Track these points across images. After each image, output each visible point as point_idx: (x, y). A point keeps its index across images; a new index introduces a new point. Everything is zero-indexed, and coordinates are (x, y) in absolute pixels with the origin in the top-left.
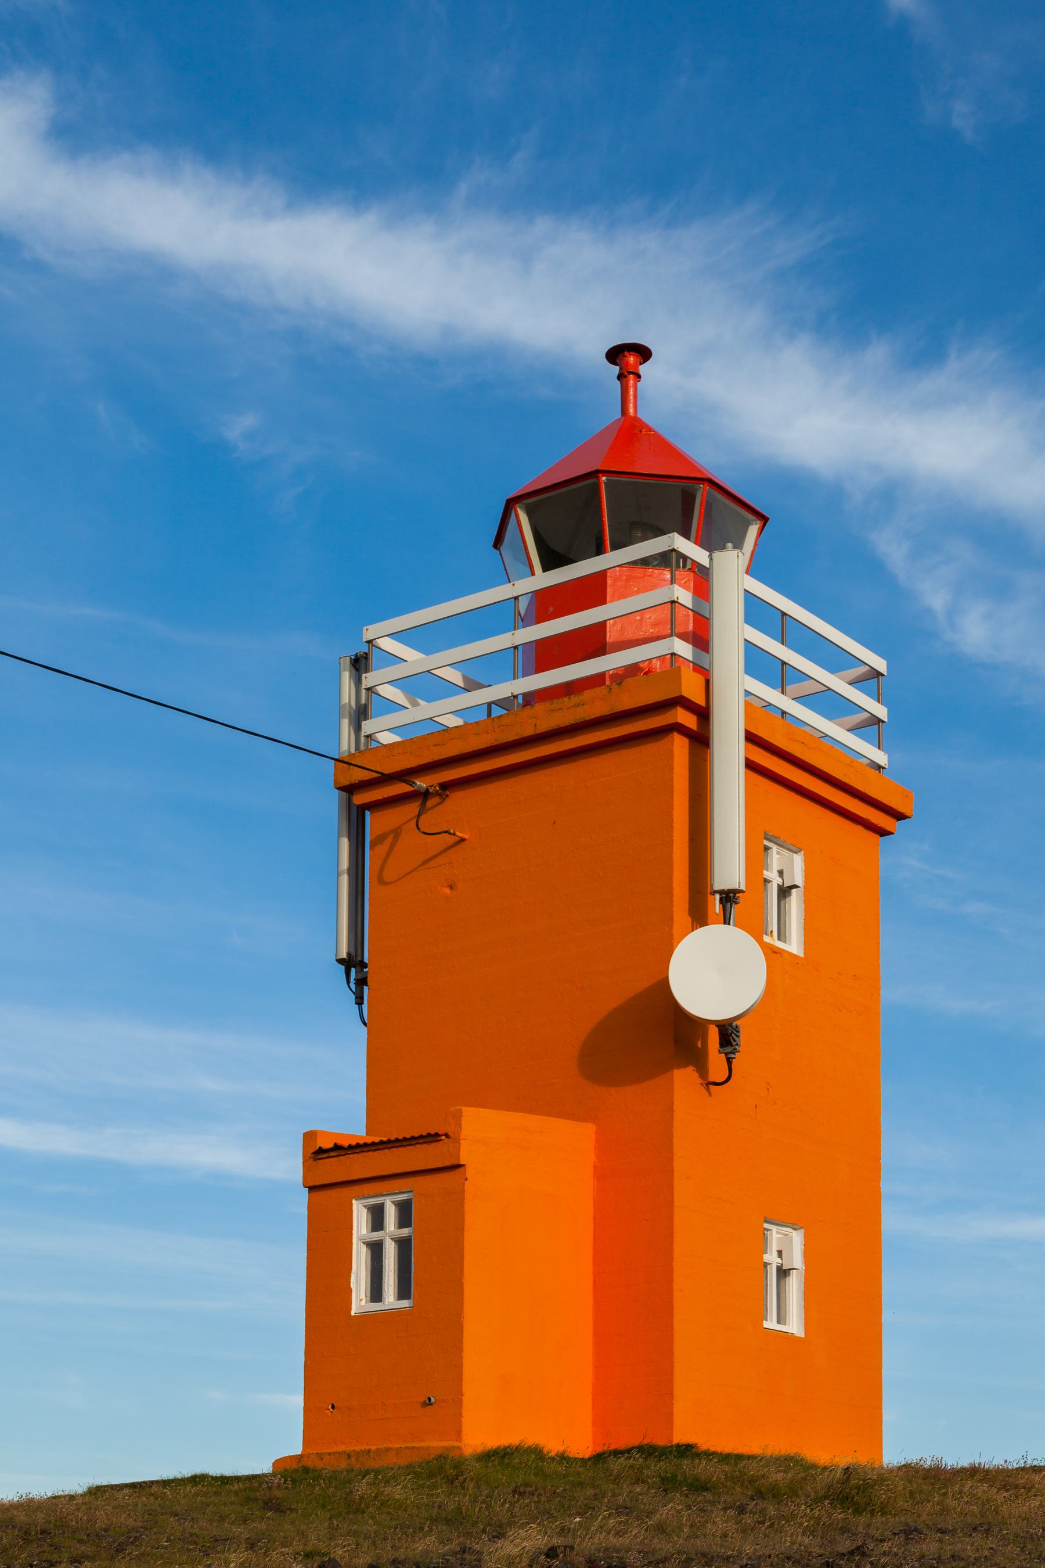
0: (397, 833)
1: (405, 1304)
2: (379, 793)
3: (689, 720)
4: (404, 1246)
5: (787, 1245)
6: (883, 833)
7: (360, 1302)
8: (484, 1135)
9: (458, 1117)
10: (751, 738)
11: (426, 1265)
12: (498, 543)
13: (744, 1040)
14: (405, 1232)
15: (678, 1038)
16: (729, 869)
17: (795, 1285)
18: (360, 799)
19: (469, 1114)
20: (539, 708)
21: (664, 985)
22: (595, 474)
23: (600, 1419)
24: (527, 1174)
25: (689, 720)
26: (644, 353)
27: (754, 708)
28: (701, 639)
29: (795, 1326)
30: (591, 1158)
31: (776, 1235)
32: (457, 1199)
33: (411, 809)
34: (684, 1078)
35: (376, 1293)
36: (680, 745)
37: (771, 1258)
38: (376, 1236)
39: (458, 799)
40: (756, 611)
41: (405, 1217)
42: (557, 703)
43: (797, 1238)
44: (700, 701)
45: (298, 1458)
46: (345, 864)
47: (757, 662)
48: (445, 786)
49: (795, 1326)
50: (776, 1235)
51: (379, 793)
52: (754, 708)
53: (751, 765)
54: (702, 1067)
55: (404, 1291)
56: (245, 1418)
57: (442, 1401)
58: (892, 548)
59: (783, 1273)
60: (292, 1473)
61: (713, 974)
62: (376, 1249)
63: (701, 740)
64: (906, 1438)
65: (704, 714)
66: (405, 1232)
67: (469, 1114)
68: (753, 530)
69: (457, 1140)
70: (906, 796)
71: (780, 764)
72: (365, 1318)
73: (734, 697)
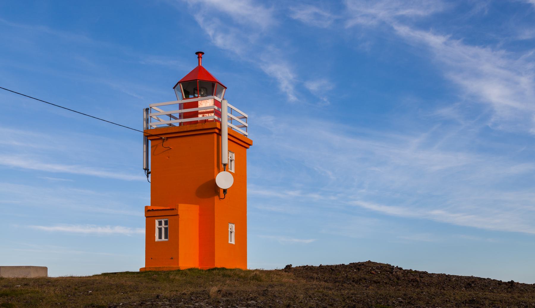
0: (157, 145)
1: (166, 240)
2: (151, 136)
3: (217, 131)
4: (166, 229)
5: (232, 227)
6: (247, 148)
7: (157, 239)
8: (182, 209)
9: (178, 206)
10: (229, 134)
11: (171, 232)
12: (174, 88)
13: (228, 191)
14: (166, 226)
15: (214, 189)
16: (225, 160)
17: (233, 234)
18: (149, 138)
19: (180, 205)
20: (188, 126)
21: (214, 181)
22: (197, 80)
23: (201, 262)
24: (188, 214)
25: (217, 131)
26: (203, 53)
27: (230, 128)
28: (218, 113)
29: (233, 242)
30: (198, 212)
31: (230, 225)
32: (177, 221)
33: (160, 141)
34: (216, 198)
35: (160, 237)
36: (215, 135)
37: (230, 230)
38: (160, 227)
39: (170, 140)
40: (231, 111)
41: (166, 223)
42: (191, 125)
43: (234, 226)
44: (219, 128)
45: (145, 268)
46: (145, 150)
47: (231, 120)
48: (167, 138)
49: (233, 242)
50: (230, 225)
51: (151, 136)
52: (230, 128)
53: (229, 139)
54: (219, 196)
55: (166, 237)
56: (135, 261)
57: (175, 258)
58: (199, 19)
59: (231, 232)
60: (142, 272)
61: (224, 180)
62: (160, 230)
63: (219, 134)
64: (253, 263)
65: (220, 130)
66: (166, 226)
67: (180, 205)
68: (224, 90)
69: (178, 210)
70: (252, 141)
71: (234, 138)
72: (158, 242)
73: (226, 125)
